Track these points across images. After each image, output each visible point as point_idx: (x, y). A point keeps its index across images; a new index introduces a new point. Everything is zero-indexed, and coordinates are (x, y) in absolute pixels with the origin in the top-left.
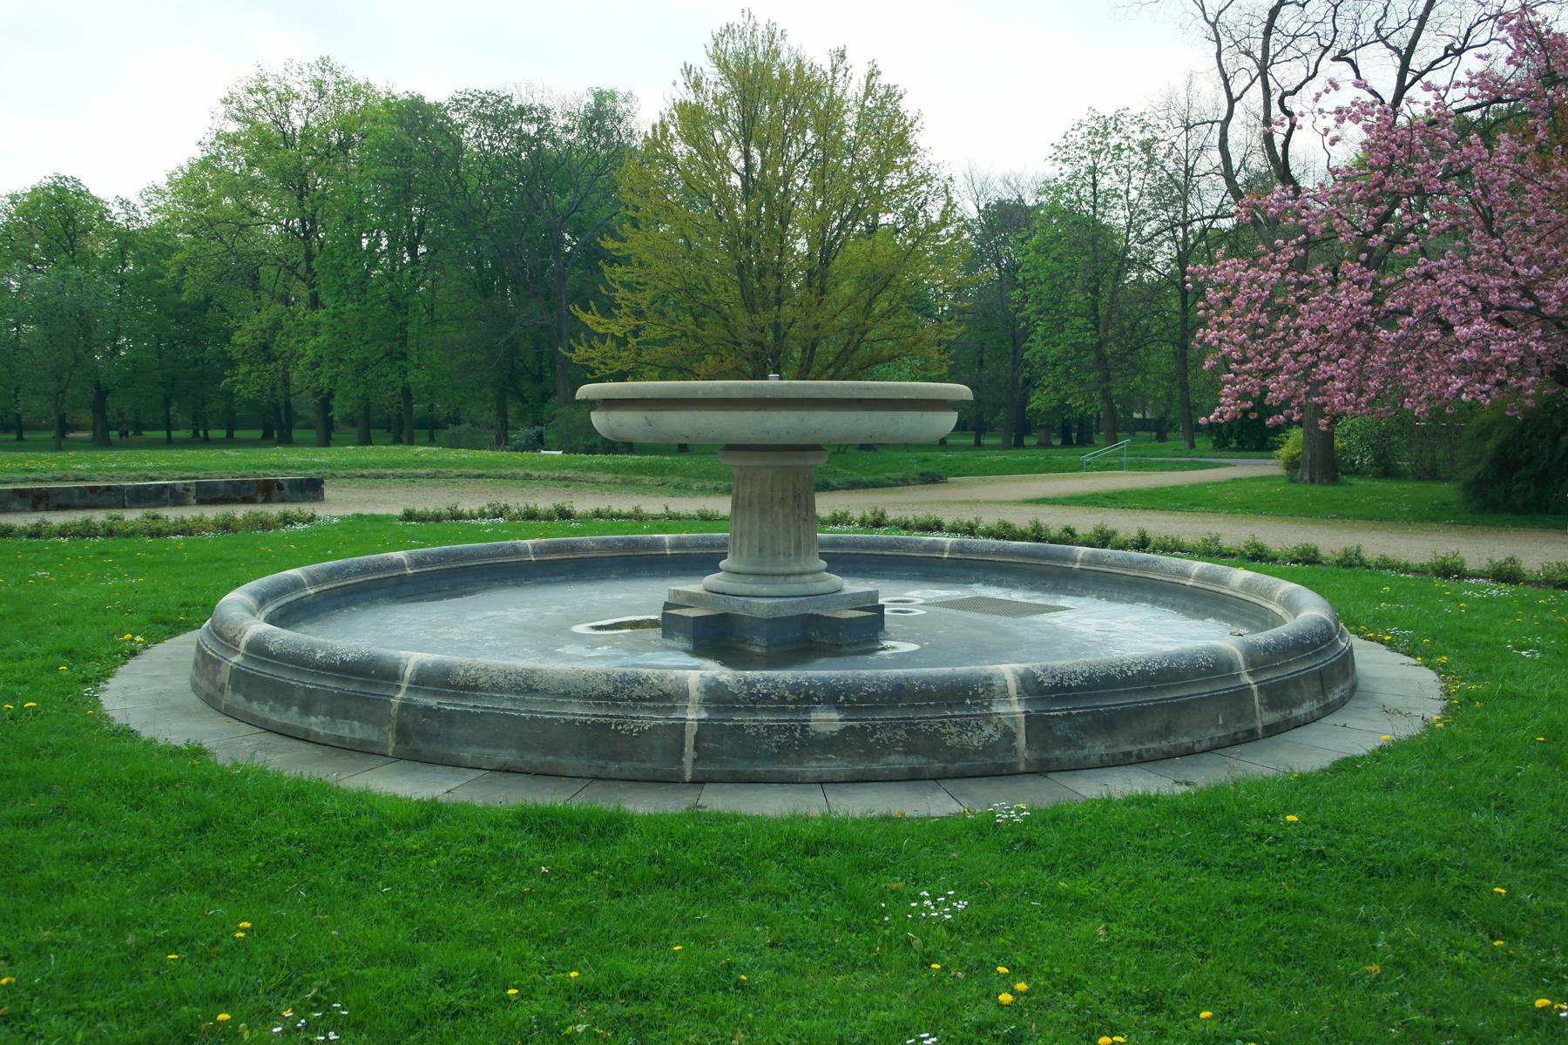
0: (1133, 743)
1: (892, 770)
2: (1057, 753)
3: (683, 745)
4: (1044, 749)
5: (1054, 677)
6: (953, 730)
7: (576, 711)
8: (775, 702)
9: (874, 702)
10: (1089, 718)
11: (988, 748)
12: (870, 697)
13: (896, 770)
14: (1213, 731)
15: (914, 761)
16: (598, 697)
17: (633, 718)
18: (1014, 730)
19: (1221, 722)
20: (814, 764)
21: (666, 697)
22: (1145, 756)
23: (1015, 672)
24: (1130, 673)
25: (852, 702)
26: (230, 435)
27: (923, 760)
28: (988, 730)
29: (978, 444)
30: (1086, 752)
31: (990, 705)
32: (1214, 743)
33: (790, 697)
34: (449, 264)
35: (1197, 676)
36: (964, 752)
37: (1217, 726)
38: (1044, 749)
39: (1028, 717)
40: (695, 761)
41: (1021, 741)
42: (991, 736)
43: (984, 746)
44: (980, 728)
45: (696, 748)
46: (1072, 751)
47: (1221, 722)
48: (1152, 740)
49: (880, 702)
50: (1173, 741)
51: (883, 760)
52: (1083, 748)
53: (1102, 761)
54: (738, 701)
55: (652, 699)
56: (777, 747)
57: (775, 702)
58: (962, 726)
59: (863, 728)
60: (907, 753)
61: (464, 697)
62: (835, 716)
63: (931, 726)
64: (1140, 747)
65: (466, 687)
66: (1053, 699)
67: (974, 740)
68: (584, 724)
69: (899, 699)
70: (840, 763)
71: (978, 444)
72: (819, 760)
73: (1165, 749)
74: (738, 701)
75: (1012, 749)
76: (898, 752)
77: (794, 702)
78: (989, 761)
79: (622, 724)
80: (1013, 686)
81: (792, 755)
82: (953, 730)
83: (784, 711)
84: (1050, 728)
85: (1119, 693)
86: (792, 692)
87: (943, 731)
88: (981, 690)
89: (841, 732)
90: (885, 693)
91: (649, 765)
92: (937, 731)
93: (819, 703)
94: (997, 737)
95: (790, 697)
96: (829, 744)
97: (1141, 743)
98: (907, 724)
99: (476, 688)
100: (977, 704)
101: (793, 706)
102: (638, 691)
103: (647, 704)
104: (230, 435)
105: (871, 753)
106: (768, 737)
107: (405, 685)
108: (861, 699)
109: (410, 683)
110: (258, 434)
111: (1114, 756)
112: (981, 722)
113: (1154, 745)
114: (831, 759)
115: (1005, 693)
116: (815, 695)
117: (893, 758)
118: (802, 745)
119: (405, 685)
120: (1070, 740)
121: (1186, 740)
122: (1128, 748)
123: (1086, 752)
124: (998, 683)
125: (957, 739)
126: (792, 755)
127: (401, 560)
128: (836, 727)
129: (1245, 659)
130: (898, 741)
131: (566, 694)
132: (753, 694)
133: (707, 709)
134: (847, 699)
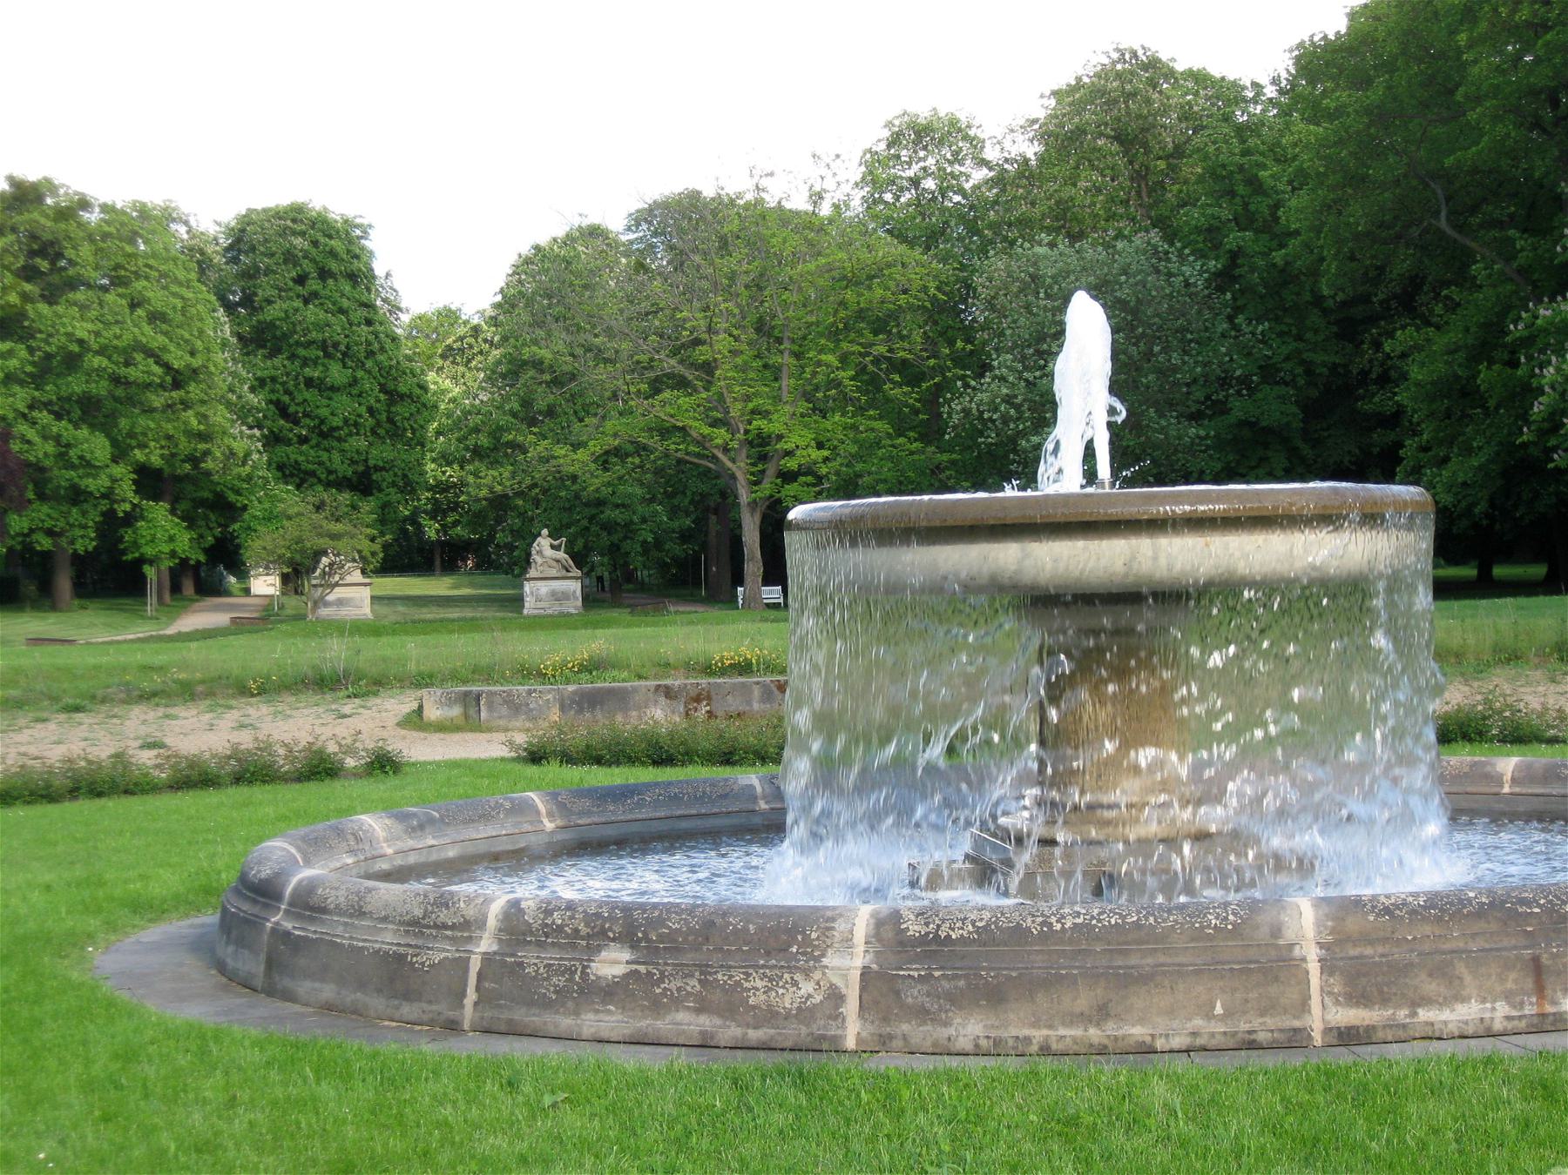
0: (1035, 1025)
1: (680, 1033)
2: (905, 1027)
3: (466, 985)
4: (886, 1020)
6: (759, 984)
7: (388, 939)
8: (568, 936)
9: (676, 941)
10: (962, 983)
11: (805, 1013)
13: (684, 1032)
14: (1198, 1022)
15: (706, 1022)
16: (409, 924)
17: (429, 949)
18: (844, 991)
19: (1219, 1010)
20: (591, 1016)
22: (1054, 1046)
24: (1058, 927)
26: (1485, 571)
27: (718, 1021)
28: (807, 987)
30: (952, 1031)
31: (823, 955)
32: (1199, 1042)
33: (584, 930)
36: (770, 1015)
37: (1209, 1015)
38: (886, 1020)
39: (865, 973)
40: (476, 1004)
41: (851, 1007)
42: (810, 996)
43: (799, 1008)
44: (795, 984)
45: (478, 989)
46: (929, 1028)
47: (1219, 1010)
48: (1071, 1024)
50: (1111, 1028)
51: (668, 1018)
52: (946, 1024)
53: (977, 1046)
54: (531, 933)
55: (453, 927)
56: (556, 992)
57: (568, 936)
58: (771, 980)
60: (699, 1011)
62: (626, 955)
64: (1045, 1032)
67: (788, 1000)
68: (387, 953)
70: (620, 1017)
72: (597, 1011)
73: (1096, 1041)
74: (531, 933)
75: (838, 1017)
76: (688, 1008)
78: (804, 1030)
79: (416, 956)
81: (570, 1004)
82: (759, 984)
83: (573, 946)
84: (897, 993)
86: (587, 925)
87: (746, 985)
88: (814, 935)
89: (626, 976)
91: (434, 1007)
92: (738, 983)
93: (613, 940)
94: (818, 999)
96: (610, 992)
97: (1050, 1027)
100: (805, 954)
101: (584, 943)
103: (449, 933)
104: (1485, 571)
105: (657, 1007)
106: (547, 979)
110: (1539, 571)
111: (997, 1042)
112: (798, 977)
113: (1077, 1032)
114: (609, 1012)
116: (610, 929)
117: (681, 1016)
118: (581, 992)
120: (928, 1012)
121: (1138, 1032)
122: (1026, 1032)
123: (952, 1031)
125: (763, 997)
126: (570, 1004)
128: (619, 970)
130: (689, 994)
132: (547, 925)
134: (646, 938)
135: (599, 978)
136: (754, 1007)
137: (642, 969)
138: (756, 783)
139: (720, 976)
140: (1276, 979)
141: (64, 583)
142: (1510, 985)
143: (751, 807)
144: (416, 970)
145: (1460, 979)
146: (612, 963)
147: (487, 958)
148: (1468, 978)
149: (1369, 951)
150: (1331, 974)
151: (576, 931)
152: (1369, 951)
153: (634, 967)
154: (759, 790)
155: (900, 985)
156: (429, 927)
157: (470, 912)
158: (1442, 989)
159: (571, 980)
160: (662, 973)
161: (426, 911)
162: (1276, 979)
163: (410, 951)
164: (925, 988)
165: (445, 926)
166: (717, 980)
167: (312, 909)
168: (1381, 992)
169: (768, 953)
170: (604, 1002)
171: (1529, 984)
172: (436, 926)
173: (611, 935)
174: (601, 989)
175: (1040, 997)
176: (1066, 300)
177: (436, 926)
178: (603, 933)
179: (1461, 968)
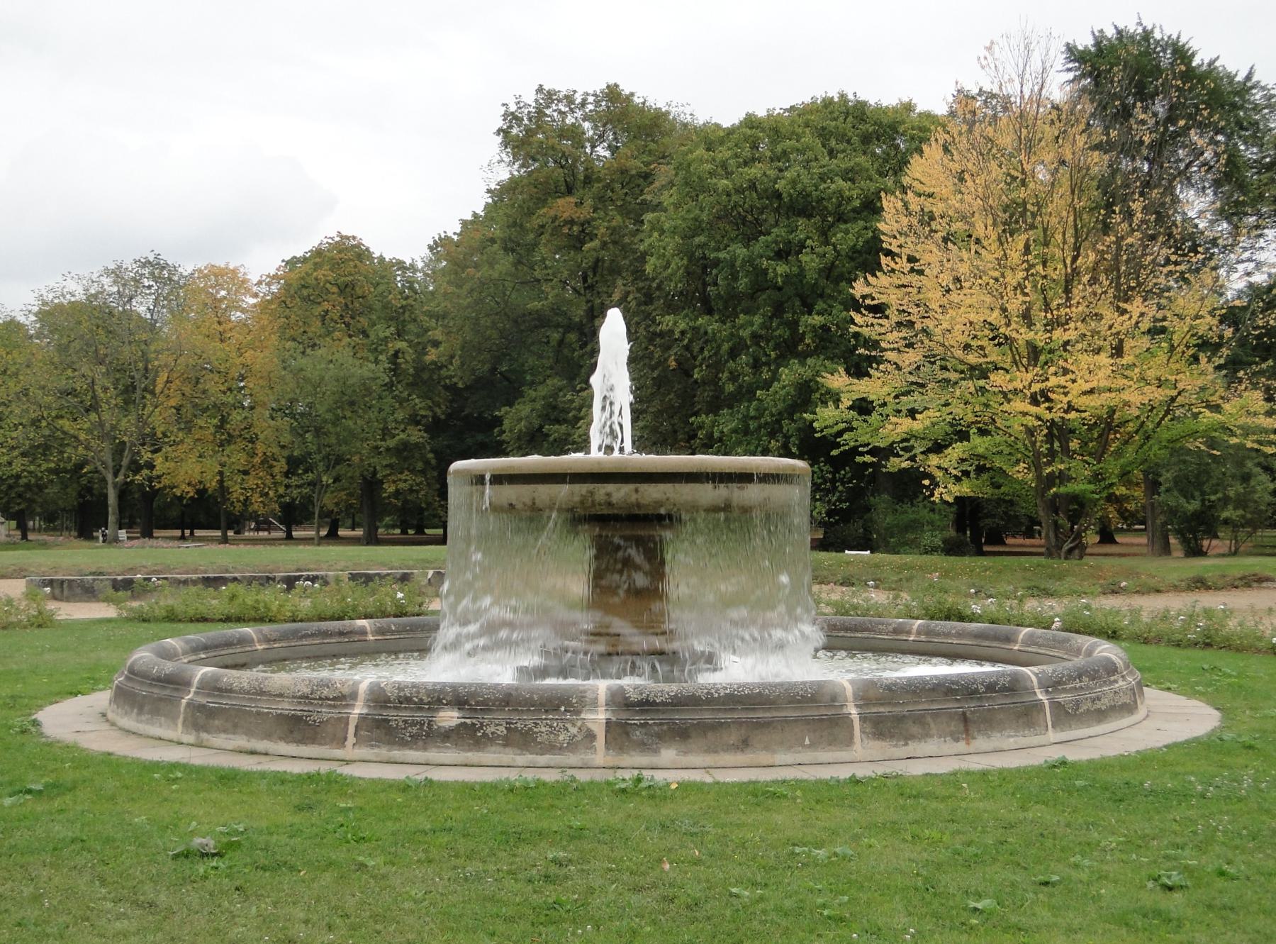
5: (641, 694)
6: (543, 729)
10: (665, 727)
12: (485, 703)
16: (301, 697)
19: (807, 742)
21: (342, 697)
23: (609, 688)
25: (471, 705)
29: (289, 537)
33: (426, 699)
34: (333, 293)
35: (790, 703)
39: (608, 723)
45: (355, 735)
47: (807, 742)
49: (493, 705)
56: (410, 736)
57: (415, 703)
59: (473, 724)
61: (222, 697)
62: (455, 714)
63: (525, 726)
65: (227, 691)
66: (637, 711)
69: (508, 704)
71: (289, 537)
74: (390, 702)
77: (429, 703)
80: (602, 698)
81: (420, 743)
82: (543, 729)
83: (421, 709)
85: (786, 721)
86: (428, 696)
87: (535, 730)
90: (497, 699)
93: (446, 705)
95: (426, 699)
98: (507, 723)
99: (231, 691)
102: (326, 692)
107: (193, 690)
108: (478, 703)
109: (198, 688)
115: (595, 702)
118: (428, 735)
119: (193, 690)
120: (645, 744)
124: (589, 695)
125: (546, 737)
127: (175, 649)
129: (854, 694)
130: (499, 736)
131: (281, 695)
133: (369, 706)
135: (439, 727)
136: (540, 743)
137: (468, 721)
138: (367, 625)
139: (519, 725)
140: (837, 724)
141: (488, 477)
142: (952, 728)
143: (363, 638)
144: (310, 725)
145: (929, 724)
146: (449, 718)
147: (363, 718)
148: (932, 725)
149: (882, 709)
150: (864, 722)
151: (421, 700)
152: (882, 709)
153: (463, 720)
154: (368, 628)
155: (629, 728)
156: (315, 699)
157: (346, 690)
158: (920, 731)
159: (421, 729)
160: (482, 724)
161: (313, 690)
162: (837, 724)
163: (305, 713)
164: (644, 731)
165: (327, 699)
166: (516, 728)
167: (220, 690)
168: (890, 732)
169: (546, 711)
170: (443, 742)
171: (962, 727)
172: (320, 699)
173: (444, 701)
174: (442, 734)
175: (710, 734)
176: (603, 315)
177: (320, 699)
178: (439, 701)
179: (929, 719)
